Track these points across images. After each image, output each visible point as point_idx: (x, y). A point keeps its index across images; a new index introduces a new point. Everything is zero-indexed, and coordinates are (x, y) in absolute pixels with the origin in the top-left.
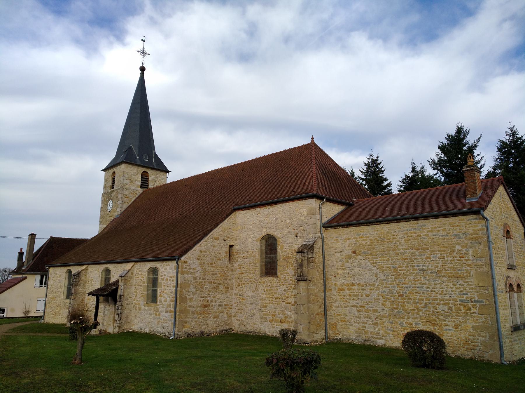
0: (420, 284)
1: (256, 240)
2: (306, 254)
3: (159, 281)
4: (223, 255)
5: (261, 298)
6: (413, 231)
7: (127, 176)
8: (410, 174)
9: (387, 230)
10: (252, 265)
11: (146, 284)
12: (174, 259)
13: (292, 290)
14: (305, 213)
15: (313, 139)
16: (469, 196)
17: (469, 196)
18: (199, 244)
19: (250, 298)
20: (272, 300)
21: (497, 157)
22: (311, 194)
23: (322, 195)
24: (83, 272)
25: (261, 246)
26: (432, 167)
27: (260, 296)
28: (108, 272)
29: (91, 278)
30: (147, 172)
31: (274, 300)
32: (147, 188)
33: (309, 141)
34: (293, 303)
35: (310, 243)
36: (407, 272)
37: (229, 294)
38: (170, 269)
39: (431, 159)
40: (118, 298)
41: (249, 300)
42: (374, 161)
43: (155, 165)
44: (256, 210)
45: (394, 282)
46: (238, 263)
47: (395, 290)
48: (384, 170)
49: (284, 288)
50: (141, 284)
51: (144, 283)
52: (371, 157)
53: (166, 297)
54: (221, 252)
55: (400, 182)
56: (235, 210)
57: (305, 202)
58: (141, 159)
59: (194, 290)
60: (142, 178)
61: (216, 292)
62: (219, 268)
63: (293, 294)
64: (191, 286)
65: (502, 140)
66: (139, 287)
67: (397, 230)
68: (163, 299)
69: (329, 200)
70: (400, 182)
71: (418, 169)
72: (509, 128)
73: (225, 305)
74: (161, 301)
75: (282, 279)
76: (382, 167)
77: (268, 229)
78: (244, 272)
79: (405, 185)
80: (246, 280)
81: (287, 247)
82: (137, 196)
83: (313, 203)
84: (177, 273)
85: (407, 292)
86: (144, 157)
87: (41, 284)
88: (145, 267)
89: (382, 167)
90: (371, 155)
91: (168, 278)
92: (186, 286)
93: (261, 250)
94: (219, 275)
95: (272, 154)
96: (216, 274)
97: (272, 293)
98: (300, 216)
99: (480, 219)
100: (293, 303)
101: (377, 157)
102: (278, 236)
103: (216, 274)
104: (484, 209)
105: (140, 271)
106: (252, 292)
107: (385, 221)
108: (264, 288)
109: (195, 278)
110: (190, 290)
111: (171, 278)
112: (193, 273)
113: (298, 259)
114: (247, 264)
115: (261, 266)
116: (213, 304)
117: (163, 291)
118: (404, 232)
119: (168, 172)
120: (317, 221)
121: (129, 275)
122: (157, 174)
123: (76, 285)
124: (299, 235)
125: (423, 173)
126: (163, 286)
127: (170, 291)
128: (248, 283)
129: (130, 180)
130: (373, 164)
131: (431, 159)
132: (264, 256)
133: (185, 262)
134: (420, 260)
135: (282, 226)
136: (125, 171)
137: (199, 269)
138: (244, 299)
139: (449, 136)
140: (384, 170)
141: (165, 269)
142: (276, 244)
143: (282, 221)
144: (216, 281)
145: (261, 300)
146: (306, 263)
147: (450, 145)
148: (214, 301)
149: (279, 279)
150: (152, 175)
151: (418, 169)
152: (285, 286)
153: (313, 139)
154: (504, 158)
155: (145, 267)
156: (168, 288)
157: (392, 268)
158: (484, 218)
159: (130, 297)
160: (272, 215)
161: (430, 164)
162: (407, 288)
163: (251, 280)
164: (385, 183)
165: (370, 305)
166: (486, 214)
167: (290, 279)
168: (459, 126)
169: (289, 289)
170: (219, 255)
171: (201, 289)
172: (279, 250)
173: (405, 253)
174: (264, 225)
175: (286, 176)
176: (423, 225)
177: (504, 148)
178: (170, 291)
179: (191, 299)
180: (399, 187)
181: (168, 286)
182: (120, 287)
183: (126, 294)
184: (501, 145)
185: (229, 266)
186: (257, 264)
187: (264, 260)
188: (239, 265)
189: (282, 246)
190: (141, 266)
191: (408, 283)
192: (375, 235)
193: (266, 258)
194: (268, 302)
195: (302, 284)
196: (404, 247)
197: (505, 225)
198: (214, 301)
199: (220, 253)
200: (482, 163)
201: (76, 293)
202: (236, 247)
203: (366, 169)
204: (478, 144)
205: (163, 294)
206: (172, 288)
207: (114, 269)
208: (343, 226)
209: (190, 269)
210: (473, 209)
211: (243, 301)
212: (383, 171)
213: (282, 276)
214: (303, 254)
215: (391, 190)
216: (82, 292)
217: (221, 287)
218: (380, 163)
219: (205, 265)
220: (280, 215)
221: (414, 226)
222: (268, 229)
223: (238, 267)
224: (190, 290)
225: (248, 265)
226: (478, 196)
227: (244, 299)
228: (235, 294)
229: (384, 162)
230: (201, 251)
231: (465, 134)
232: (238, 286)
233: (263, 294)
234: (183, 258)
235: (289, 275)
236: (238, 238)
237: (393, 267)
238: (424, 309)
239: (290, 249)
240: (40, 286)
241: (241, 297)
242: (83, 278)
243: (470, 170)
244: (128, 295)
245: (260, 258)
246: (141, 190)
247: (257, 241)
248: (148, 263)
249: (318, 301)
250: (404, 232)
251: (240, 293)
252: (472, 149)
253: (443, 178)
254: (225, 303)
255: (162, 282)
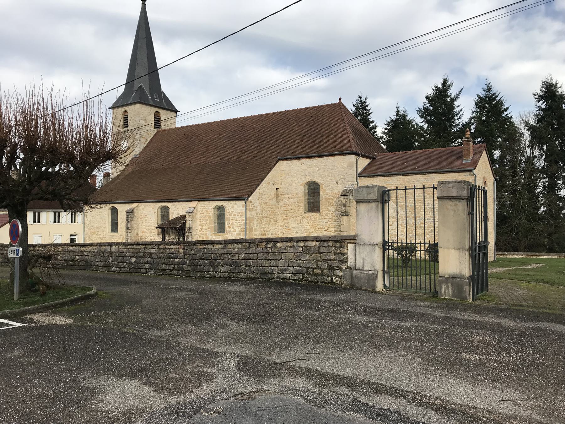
0: (428, 217)
1: (300, 185)
2: (348, 197)
3: (227, 216)
4: (273, 196)
5: (305, 228)
6: (426, 181)
7: (142, 116)
8: (394, 118)
9: (407, 180)
10: (297, 204)
11: (212, 219)
12: (244, 200)
13: (333, 222)
14: (346, 166)
15: (340, 99)
16: (465, 158)
17: (465, 158)
18: (258, 188)
19: (295, 229)
20: (315, 230)
21: (474, 110)
22: (351, 151)
23: (359, 152)
24: (136, 209)
25: (305, 190)
26: (419, 116)
27: (304, 227)
28: (165, 210)
29: (144, 214)
30: (158, 112)
31: (317, 229)
32: (160, 128)
33: (338, 101)
34: (333, 231)
35: (351, 188)
36: (420, 209)
37: (277, 226)
38: (238, 207)
39: (419, 108)
40: (186, 230)
41: (294, 230)
42: (362, 103)
43: (165, 105)
44: (300, 161)
45: (411, 216)
46: (283, 203)
47: (411, 221)
48: (372, 113)
49: (326, 220)
50: (207, 218)
51: (210, 217)
52: (360, 99)
53: (235, 228)
54: (271, 194)
55: (385, 124)
56: (280, 160)
57: (345, 158)
58: (153, 99)
59: (257, 223)
60: (155, 118)
61: (270, 224)
62: (270, 206)
63: (333, 225)
64: (255, 219)
65: (479, 95)
66: (205, 221)
67: (414, 181)
68: (231, 230)
69: (363, 156)
70: (385, 124)
71: (402, 113)
72: (486, 85)
73: (275, 234)
74: (229, 231)
75: (324, 214)
76: (370, 110)
77: (311, 176)
78: (289, 209)
79: (389, 127)
80: (291, 215)
81: (329, 191)
82: (152, 136)
83: (353, 158)
84: (246, 210)
85: (420, 222)
86: (155, 97)
87: (55, 220)
88: (211, 205)
89: (370, 110)
90: (360, 97)
91: (236, 214)
92: (252, 220)
93: (305, 192)
94: (270, 212)
95: (301, 109)
96: (269, 211)
97: (315, 225)
98: (341, 168)
99: (471, 175)
100: (333, 231)
101: (366, 99)
102: (321, 182)
103: (269, 211)
104: (475, 169)
105: (204, 208)
106: (297, 224)
107: (406, 174)
108: (307, 221)
109: (257, 214)
110: (254, 223)
111: (239, 214)
112: (256, 210)
113: (342, 200)
114: (292, 203)
115: (305, 205)
116: (268, 233)
117: (232, 224)
118: (420, 182)
119: (176, 111)
120: (354, 172)
121: (195, 211)
122: (167, 114)
123: (131, 221)
124: (339, 182)
125: (405, 117)
126: (231, 220)
127: (239, 223)
128: (294, 218)
129: (145, 120)
130: (361, 106)
131: (419, 108)
132: (307, 197)
133: (251, 202)
134: (430, 201)
135: (325, 175)
136: (140, 111)
137: (259, 207)
138: (290, 230)
139: (436, 87)
140: (372, 113)
141: (232, 207)
142: (319, 188)
143: (324, 171)
144: (269, 216)
145: (305, 229)
146: (349, 203)
147: (435, 95)
148: (268, 231)
149: (321, 214)
150: (164, 114)
151: (402, 113)
152: (326, 220)
153: (340, 99)
154: (480, 111)
155: (211, 205)
156: (236, 221)
157: (409, 207)
158: (474, 175)
159: (197, 229)
160: (315, 166)
161: (418, 113)
162: (419, 220)
163: (296, 215)
164: (372, 125)
165: (392, 232)
166: (475, 172)
167: (331, 214)
168: (445, 78)
169: (330, 222)
170: (271, 196)
171: (261, 222)
172: (321, 193)
173: (420, 196)
174: (308, 173)
175: (322, 133)
176: (434, 178)
177: (480, 102)
178: (239, 223)
179: (255, 229)
180: (384, 130)
181: (236, 220)
182: (187, 221)
183: (194, 227)
184: (478, 99)
185: (277, 204)
186: (301, 204)
187: (307, 200)
188: (284, 204)
189: (324, 191)
190: (205, 204)
191: (420, 217)
192: (398, 183)
193: (308, 199)
194: (311, 231)
195: (345, 218)
196: (419, 192)
197: (484, 178)
198: (268, 231)
199: (271, 195)
200: (461, 113)
201: (132, 227)
202: (281, 190)
203: (355, 110)
204: (459, 97)
205: (231, 226)
206: (240, 221)
207: (174, 206)
208: (374, 176)
209: (254, 207)
210: (469, 169)
211: (289, 231)
212: (370, 114)
213: (324, 212)
214: (346, 196)
215: (376, 132)
216: (136, 226)
217: (272, 220)
218: (367, 105)
219: (263, 204)
220: (323, 167)
221: (427, 178)
222: (311, 176)
223: (283, 206)
224: (254, 223)
225: (293, 204)
226: (471, 159)
227: (290, 230)
228: (281, 226)
229: (373, 105)
230: (260, 194)
231: (450, 86)
232: (284, 220)
233: (307, 225)
234: (250, 199)
235: (331, 212)
236: (283, 182)
237: (410, 206)
238: (430, 233)
239: (331, 193)
240: (34, 223)
241: (287, 228)
242: (136, 214)
243: (467, 140)
244: (195, 227)
245: (304, 199)
246: (155, 130)
247: (301, 185)
248: (213, 202)
249: (355, 230)
250: (420, 182)
251: (286, 225)
252: (453, 100)
253: (426, 126)
254: (275, 233)
255: (230, 217)
